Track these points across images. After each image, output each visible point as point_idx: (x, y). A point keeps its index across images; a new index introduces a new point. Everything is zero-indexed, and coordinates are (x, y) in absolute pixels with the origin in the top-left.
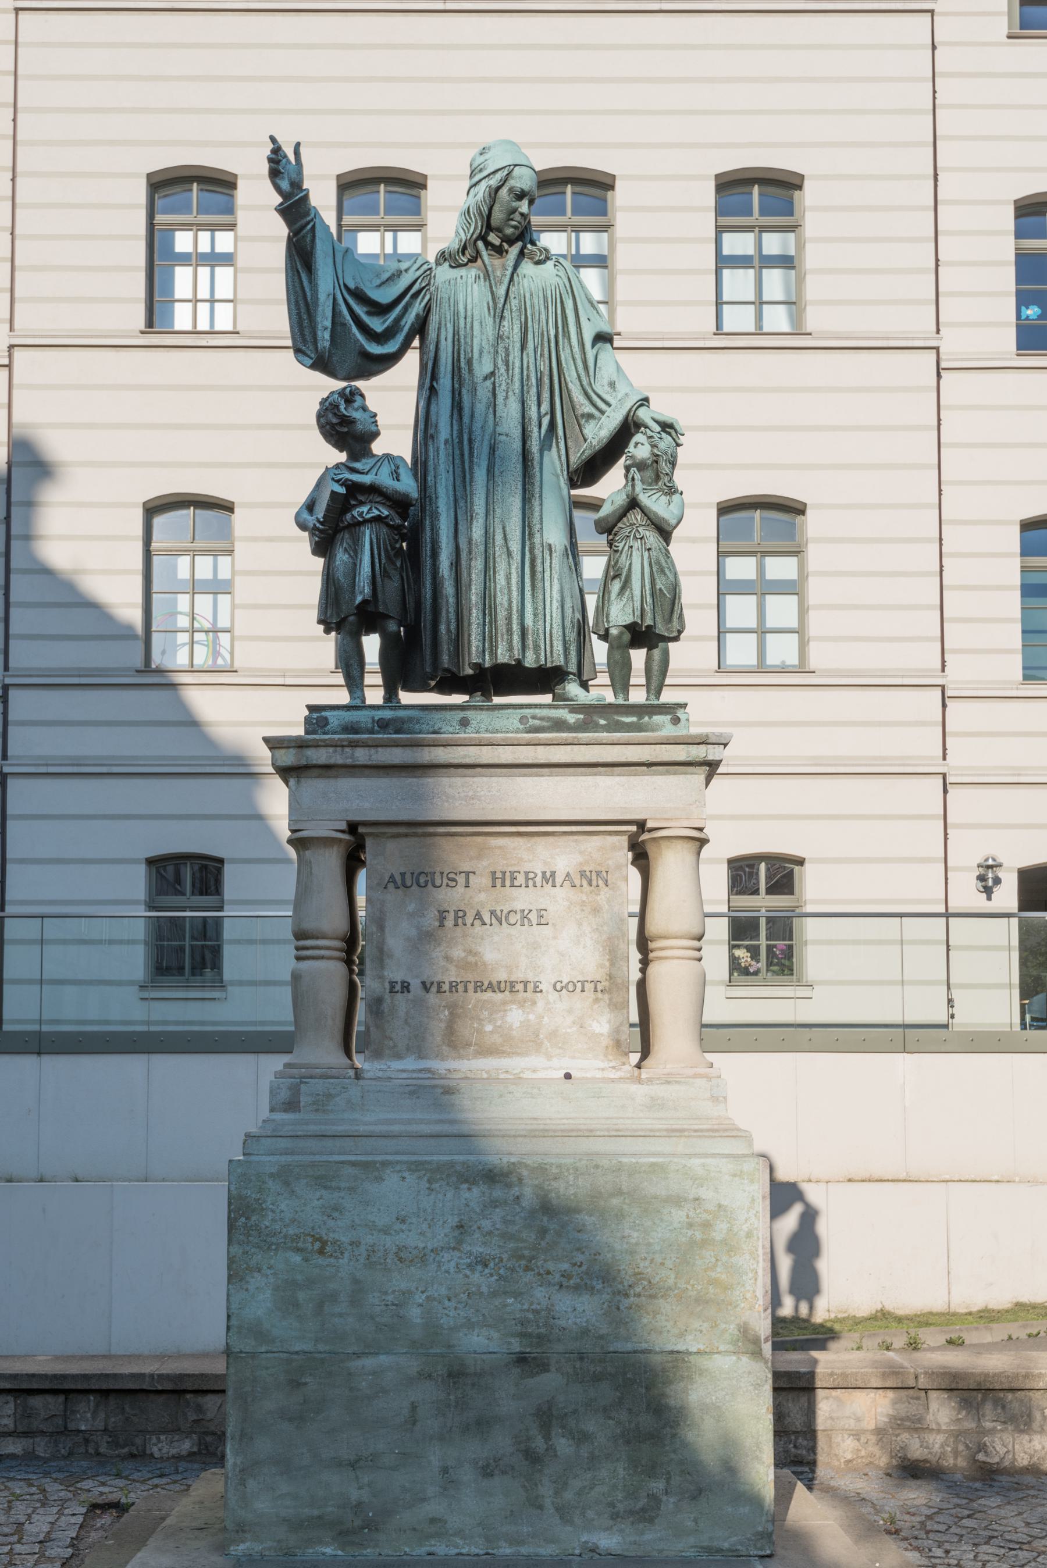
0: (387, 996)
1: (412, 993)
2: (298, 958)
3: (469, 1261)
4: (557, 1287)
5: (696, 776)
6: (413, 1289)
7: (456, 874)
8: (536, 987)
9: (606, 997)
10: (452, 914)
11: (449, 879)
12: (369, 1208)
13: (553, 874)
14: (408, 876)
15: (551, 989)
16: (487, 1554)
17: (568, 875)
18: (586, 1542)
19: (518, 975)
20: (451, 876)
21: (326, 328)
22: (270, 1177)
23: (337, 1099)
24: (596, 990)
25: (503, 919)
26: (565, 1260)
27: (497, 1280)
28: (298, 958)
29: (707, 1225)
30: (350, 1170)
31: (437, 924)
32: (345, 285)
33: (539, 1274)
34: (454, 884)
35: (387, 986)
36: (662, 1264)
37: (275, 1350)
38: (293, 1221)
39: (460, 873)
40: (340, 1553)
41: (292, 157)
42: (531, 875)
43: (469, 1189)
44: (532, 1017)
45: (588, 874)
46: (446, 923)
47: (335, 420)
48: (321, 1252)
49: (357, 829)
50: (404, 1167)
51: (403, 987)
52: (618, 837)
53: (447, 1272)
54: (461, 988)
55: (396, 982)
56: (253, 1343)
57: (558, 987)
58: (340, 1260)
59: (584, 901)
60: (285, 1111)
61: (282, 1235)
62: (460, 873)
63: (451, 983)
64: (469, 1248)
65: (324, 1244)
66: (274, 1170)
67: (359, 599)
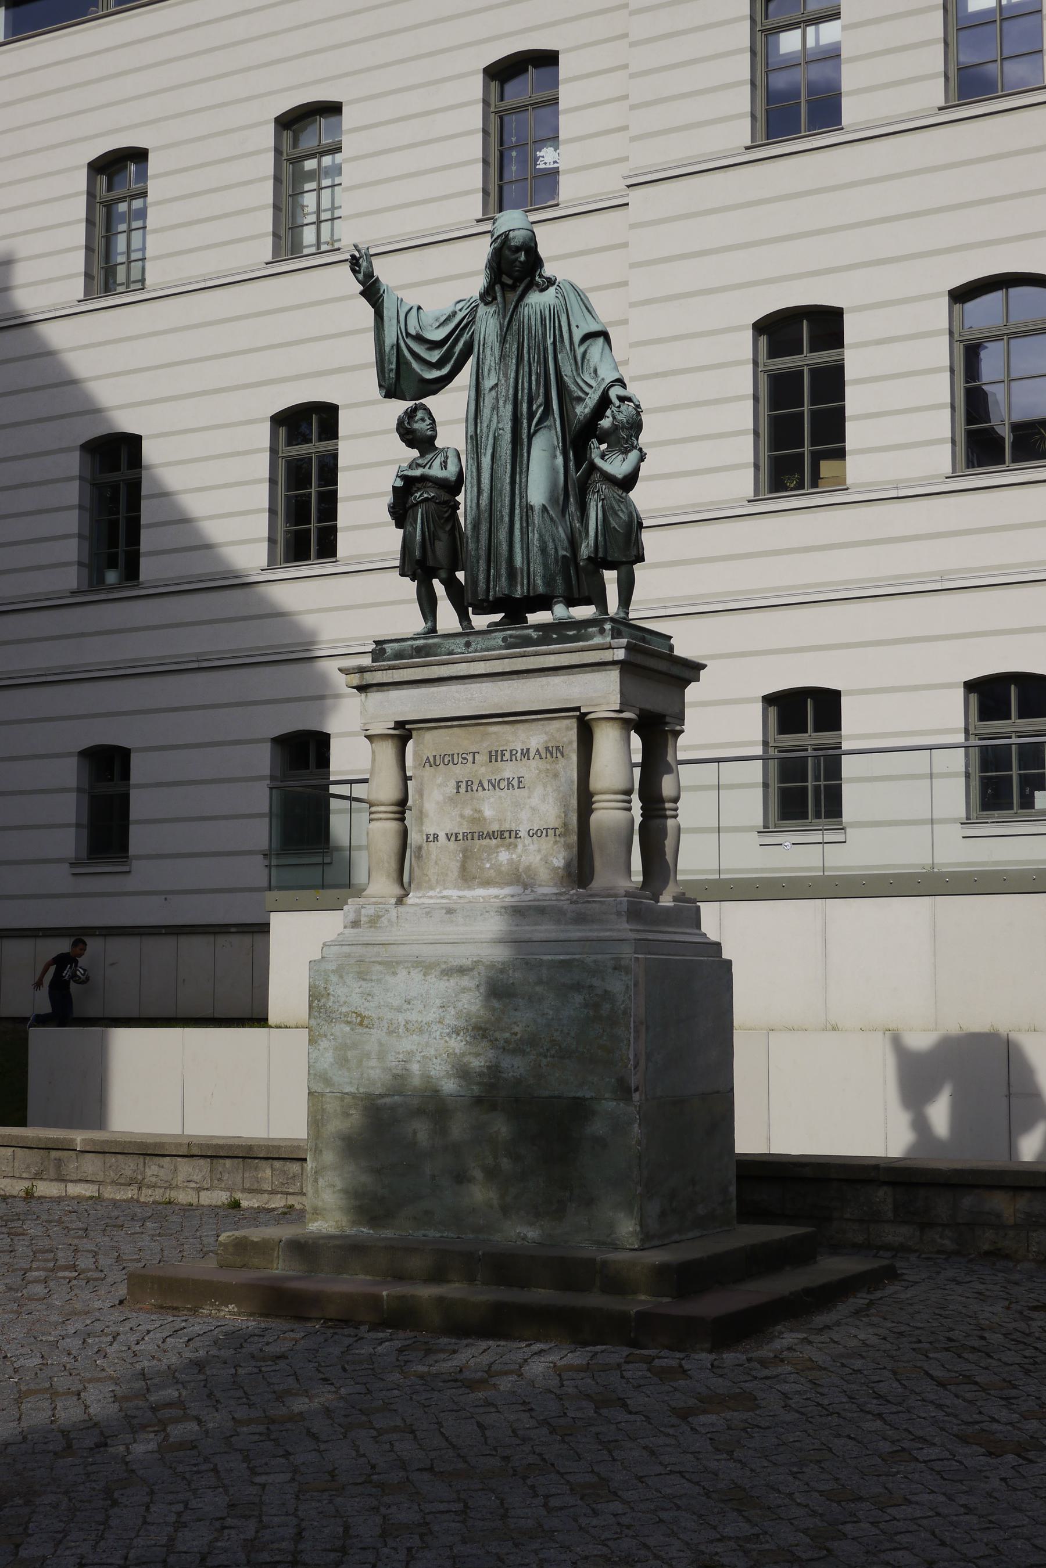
0: (425, 844)
3: (448, 1031)
4: (502, 1050)
5: (613, 672)
6: (415, 1051)
8: (517, 834)
9: (562, 840)
10: (464, 783)
11: (462, 758)
12: (388, 994)
13: (528, 750)
14: (438, 757)
16: (458, 1238)
17: (538, 750)
18: (519, 1233)
19: (506, 826)
21: (391, 370)
23: (383, 919)
24: (555, 835)
30: (378, 968)
31: (455, 791)
32: (408, 334)
33: (491, 1041)
36: (568, 1034)
37: (335, 1091)
38: (345, 1003)
40: (371, 1232)
42: (514, 752)
43: (448, 980)
44: (514, 856)
45: (551, 749)
46: (461, 790)
48: (361, 1024)
50: (410, 965)
51: (434, 838)
52: (570, 721)
53: (435, 1039)
56: (322, 1086)
57: (531, 834)
59: (548, 769)
63: (463, 833)
64: (448, 1022)
65: (363, 1018)
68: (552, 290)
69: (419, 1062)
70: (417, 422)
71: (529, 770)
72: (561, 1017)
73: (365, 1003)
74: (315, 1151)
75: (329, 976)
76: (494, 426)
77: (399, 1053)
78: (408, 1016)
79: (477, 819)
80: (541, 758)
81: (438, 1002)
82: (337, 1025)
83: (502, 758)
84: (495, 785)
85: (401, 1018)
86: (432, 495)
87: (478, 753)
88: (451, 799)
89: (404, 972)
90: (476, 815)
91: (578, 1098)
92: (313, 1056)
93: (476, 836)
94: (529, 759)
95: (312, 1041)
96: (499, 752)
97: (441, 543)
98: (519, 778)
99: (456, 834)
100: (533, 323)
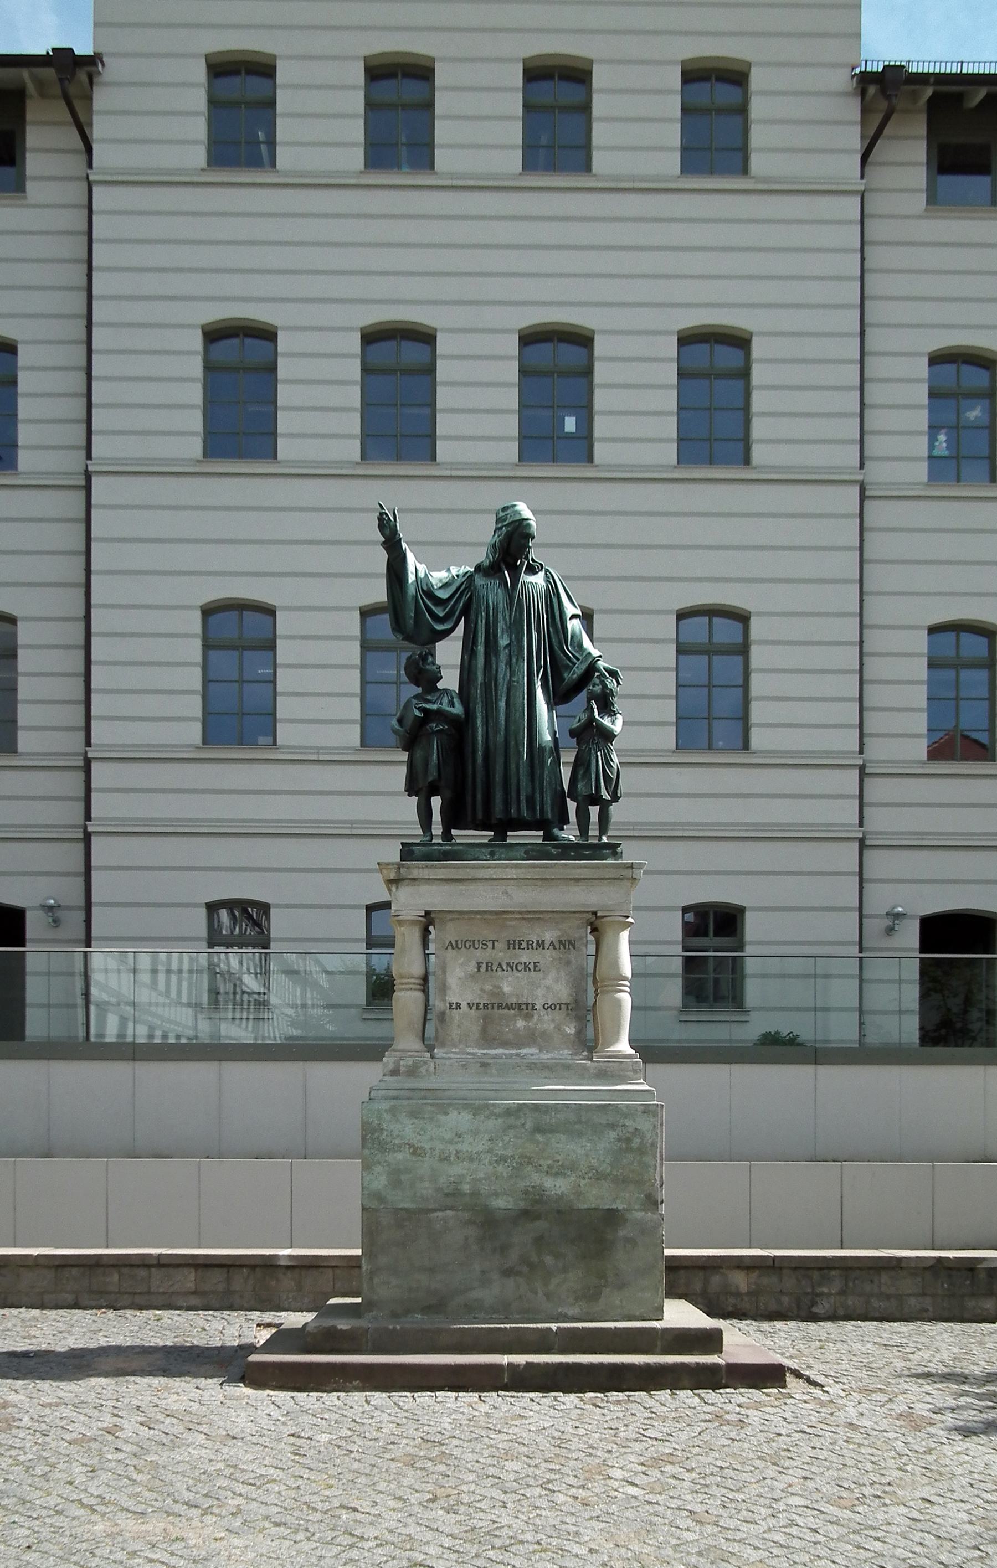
0: (448, 1011)
8: (533, 1007)
14: (459, 942)
15: (542, 1008)
35: (448, 1005)
38: (398, 1136)
42: (531, 943)
53: (484, 1165)
57: (546, 1006)
71: (545, 957)
74: (370, 1256)
77: (450, 1176)
78: (459, 1147)
79: (497, 992)
84: (513, 967)
85: (452, 1149)
88: (472, 976)
89: (456, 1113)
90: (495, 990)
93: (496, 1006)
94: (544, 948)
95: (367, 1167)
98: (534, 963)
99: (477, 1004)
100: (491, 604)
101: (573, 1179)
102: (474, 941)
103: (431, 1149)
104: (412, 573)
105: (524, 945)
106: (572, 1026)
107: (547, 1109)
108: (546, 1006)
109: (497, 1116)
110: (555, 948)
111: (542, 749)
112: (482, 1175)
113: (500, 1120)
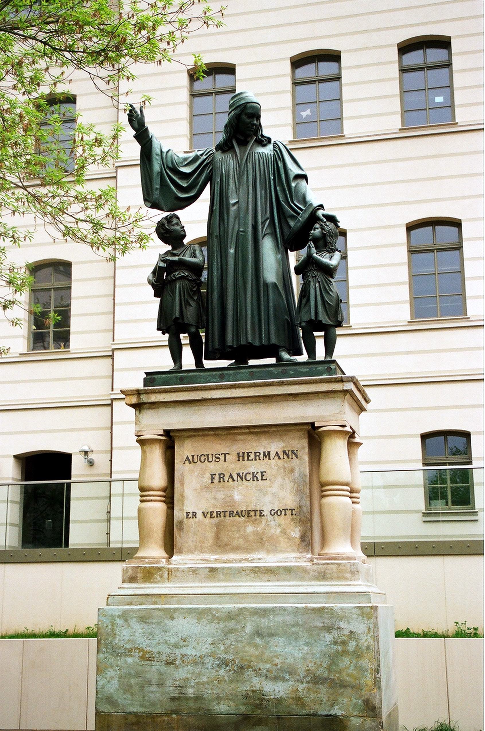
1: (197, 518)
2: (142, 501)
3: (218, 662)
7: (219, 455)
10: (217, 476)
11: (216, 457)
13: (269, 453)
14: (195, 457)
15: (269, 514)
17: (277, 453)
19: (252, 507)
20: (217, 456)
21: (157, 189)
22: (118, 617)
24: (292, 515)
25: (244, 477)
26: (269, 662)
27: (233, 673)
28: (142, 501)
29: (344, 643)
33: (255, 670)
34: (218, 460)
35: (185, 515)
36: (321, 665)
37: (120, 711)
39: (222, 454)
41: (139, 113)
42: (258, 454)
45: (287, 452)
46: (214, 481)
47: (162, 231)
49: (314, 425)
53: (207, 669)
54: (222, 515)
55: (190, 513)
57: (272, 513)
58: (153, 662)
60: (130, 582)
61: (124, 648)
62: (222, 454)
63: (217, 512)
66: (120, 613)
67: (174, 317)
68: (271, 146)
69: (193, 687)
70: (173, 225)
72: (315, 652)
73: (146, 641)
75: (115, 620)
76: (236, 229)
77: (176, 680)
78: (184, 651)
80: (190, 463)
81: (210, 640)
82: (122, 658)
83: (248, 458)
86: (187, 274)
87: (229, 454)
90: (228, 499)
91: (331, 715)
92: (101, 683)
94: (269, 459)
96: (246, 454)
97: (191, 308)
99: (211, 512)
101: (291, 683)
102: (208, 455)
103: (159, 653)
104: (157, 155)
105: (252, 456)
106: (297, 530)
107: (264, 613)
108: (273, 513)
109: (220, 620)
110: (280, 459)
111: (266, 285)
112: (205, 679)
113: (222, 625)
